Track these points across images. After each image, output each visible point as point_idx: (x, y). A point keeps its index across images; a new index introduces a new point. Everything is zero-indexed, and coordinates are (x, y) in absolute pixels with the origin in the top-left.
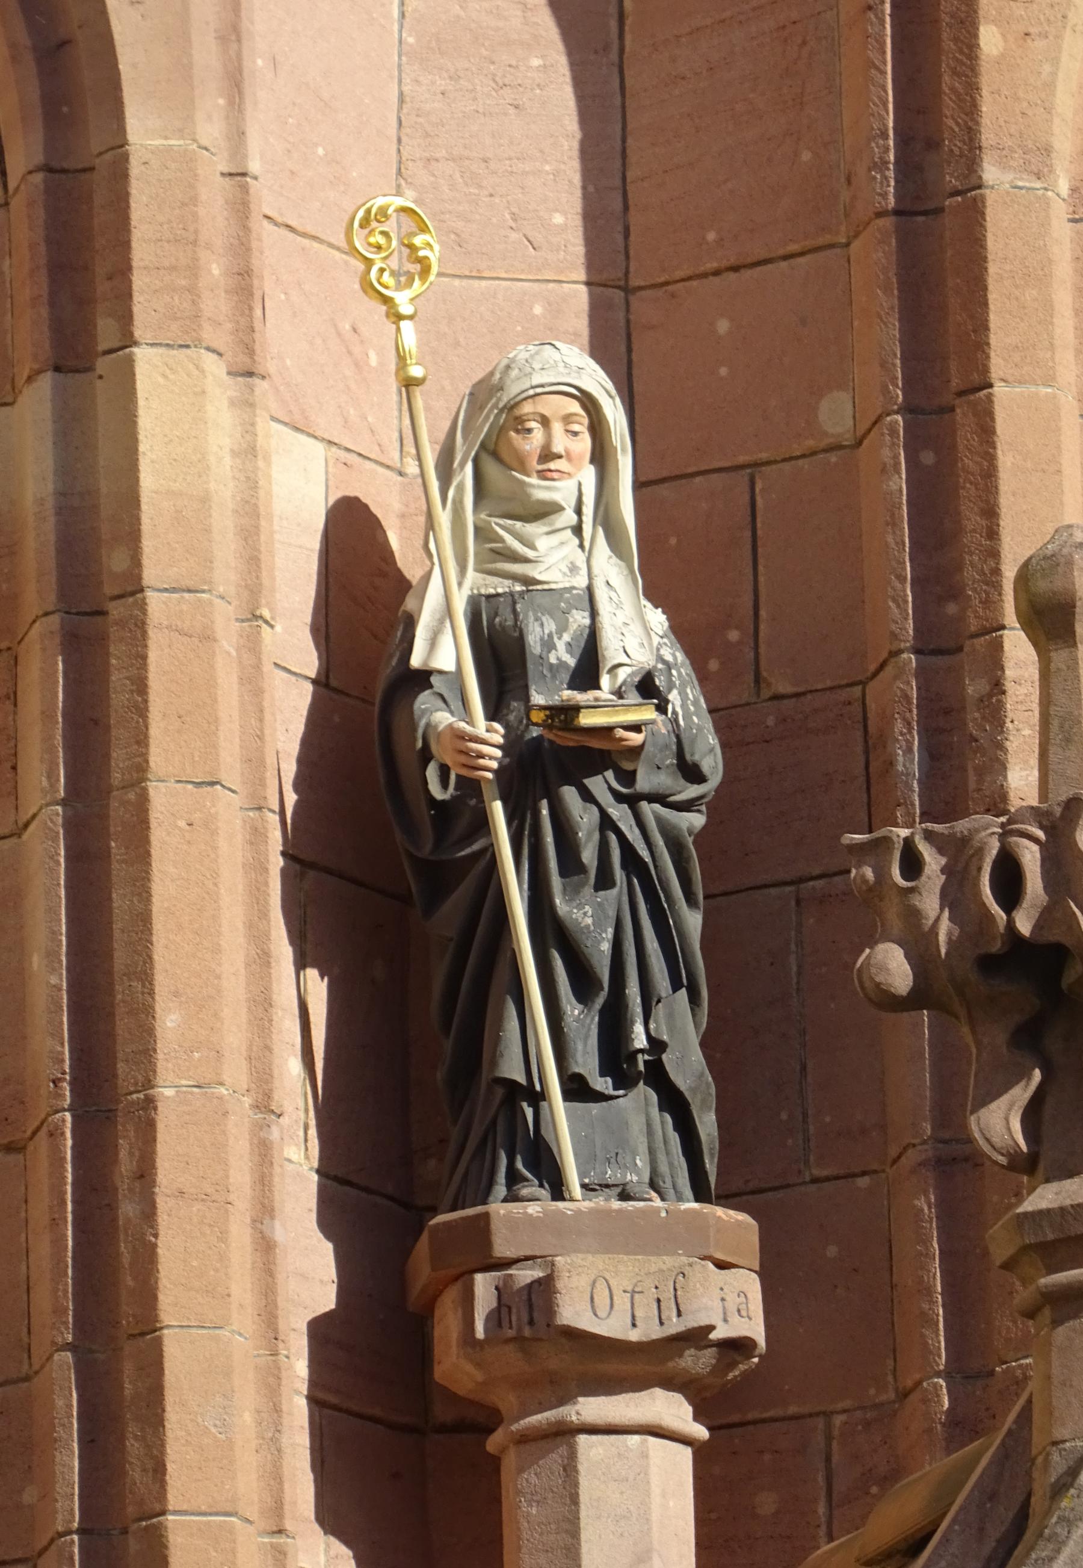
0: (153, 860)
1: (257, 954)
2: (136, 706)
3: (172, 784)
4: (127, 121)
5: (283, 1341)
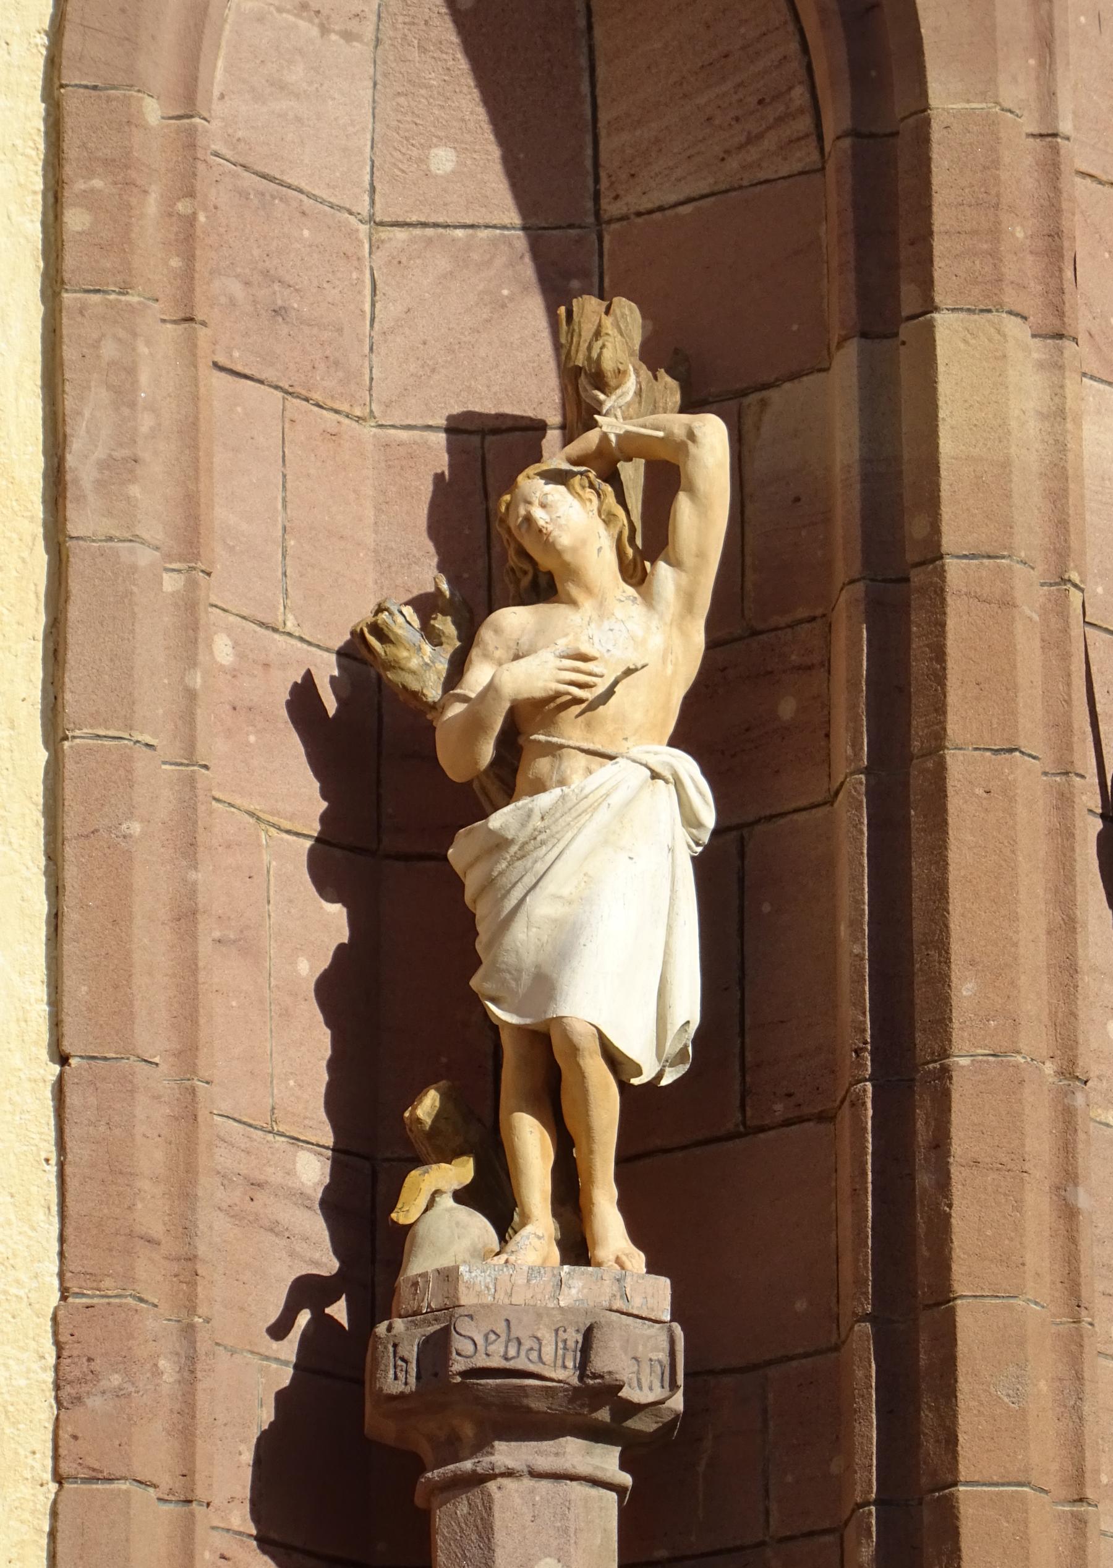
0: (950, 828)
1: (1063, 919)
2: (936, 676)
3: (969, 752)
4: (929, 85)
5: (1086, 1308)
